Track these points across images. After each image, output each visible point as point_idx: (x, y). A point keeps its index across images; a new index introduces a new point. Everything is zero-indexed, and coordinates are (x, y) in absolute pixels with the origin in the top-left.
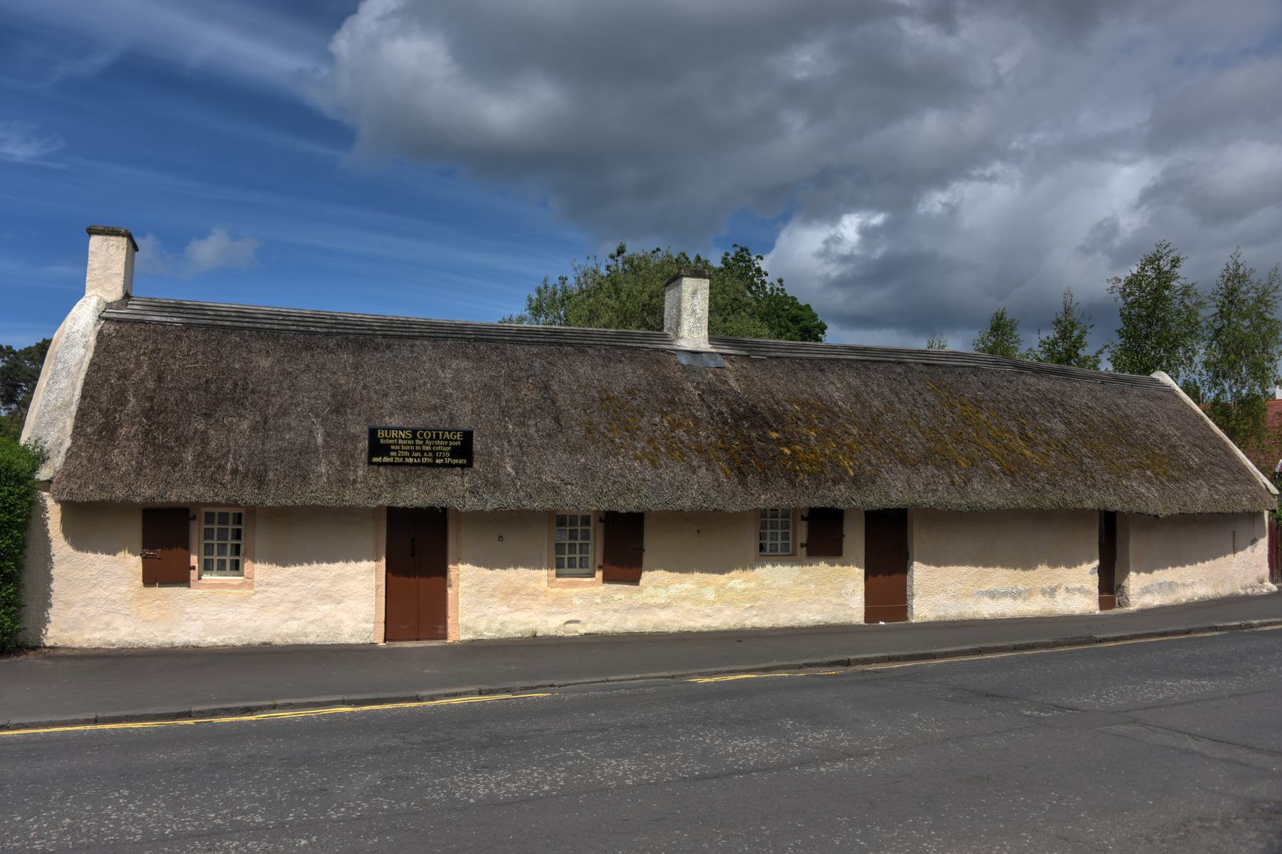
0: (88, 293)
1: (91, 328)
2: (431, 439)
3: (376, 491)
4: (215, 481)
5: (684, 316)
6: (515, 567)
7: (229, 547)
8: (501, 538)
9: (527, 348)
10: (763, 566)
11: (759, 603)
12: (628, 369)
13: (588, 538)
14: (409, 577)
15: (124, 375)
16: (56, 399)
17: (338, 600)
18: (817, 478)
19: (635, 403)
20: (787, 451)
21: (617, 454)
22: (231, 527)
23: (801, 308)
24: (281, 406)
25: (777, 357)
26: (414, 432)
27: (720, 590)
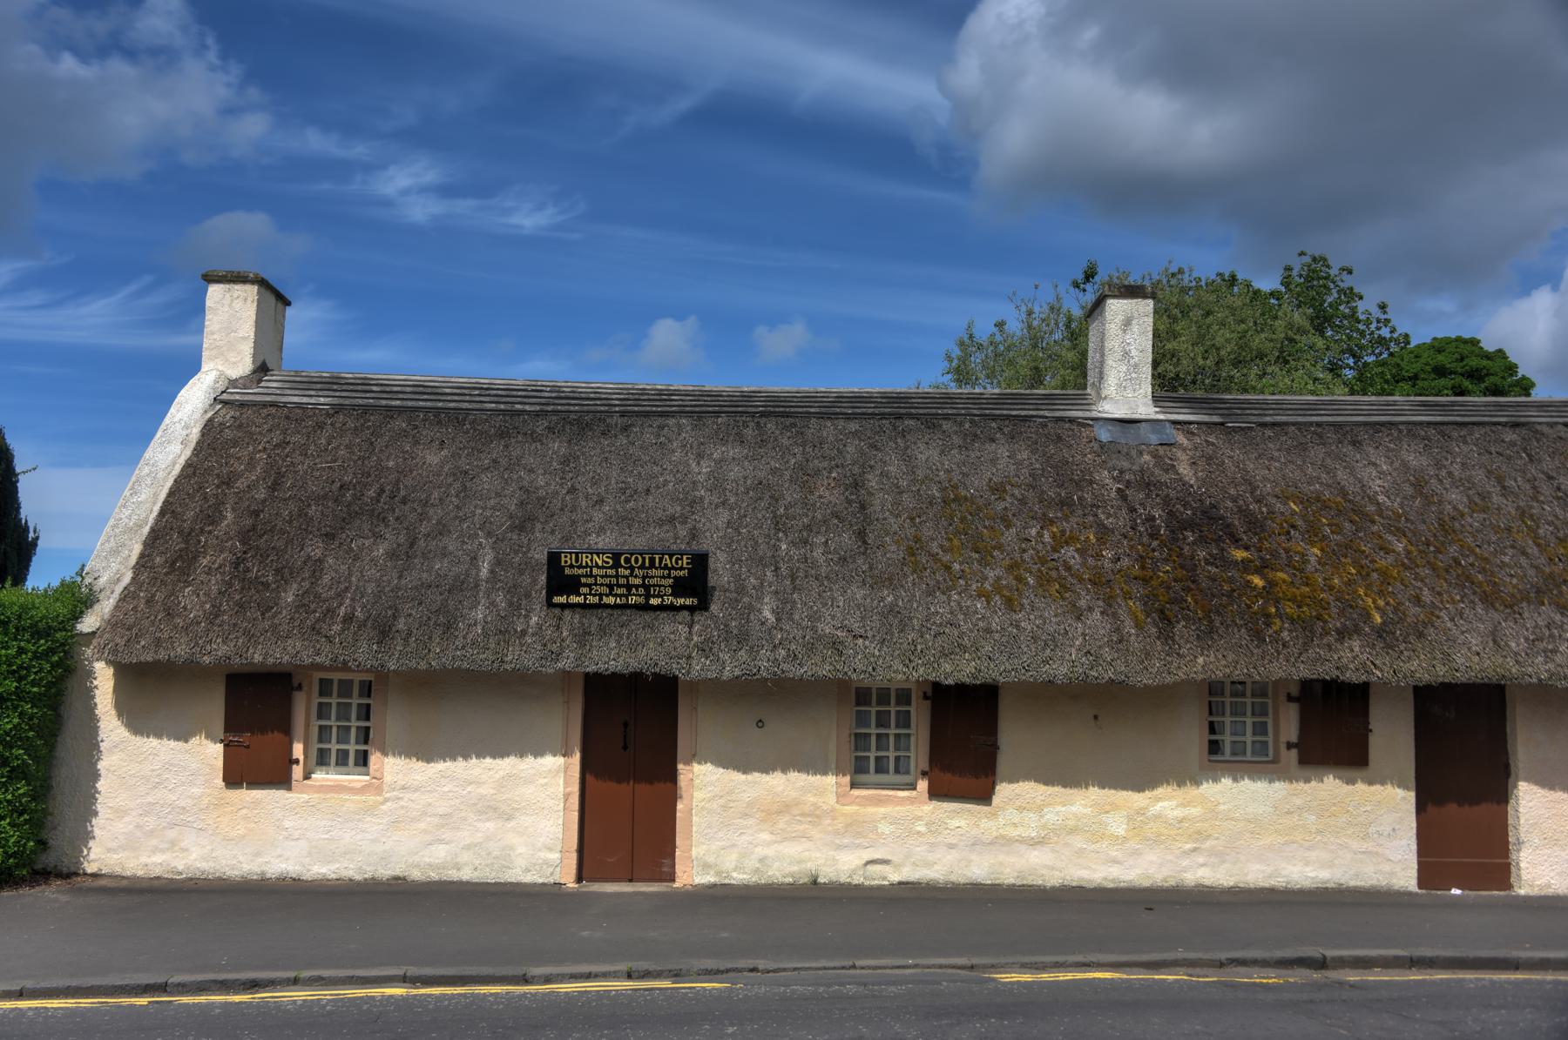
0: (205, 368)
1: (197, 415)
2: (642, 567)
3: (554, 647)
4: (319, 633)
5: (1110, 362)
6: (784, 771)
7: (353, 731)
8: (760, 723)
9: (841, 424)
10: (1216, 780)
11: (1208, 844)
12: (1003, 452)
13: (908, 726)
14: (619, 782)
15: (227, 482)
16: (129, 518)
17: (506, 813)
18: (1308, 628)
19: (1000, 506)
20: (1258, 581)
21: (949, 589)
22: (355, 701)
23: (1488, 356)
24: (439, 522)
25: (1274, 424)
26: (616, 556)
27: (1137, 820)
